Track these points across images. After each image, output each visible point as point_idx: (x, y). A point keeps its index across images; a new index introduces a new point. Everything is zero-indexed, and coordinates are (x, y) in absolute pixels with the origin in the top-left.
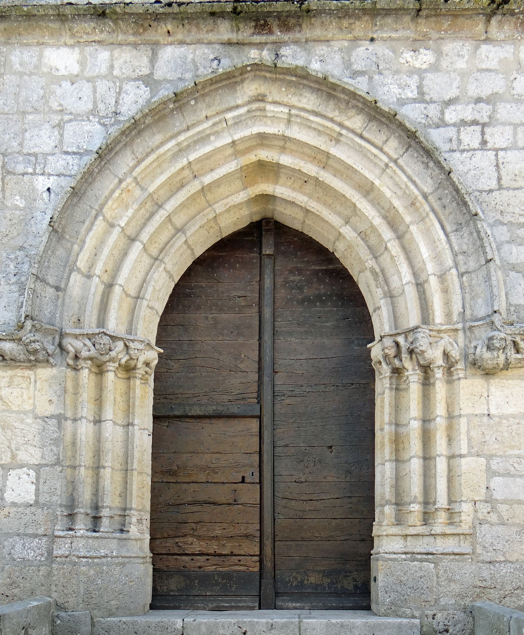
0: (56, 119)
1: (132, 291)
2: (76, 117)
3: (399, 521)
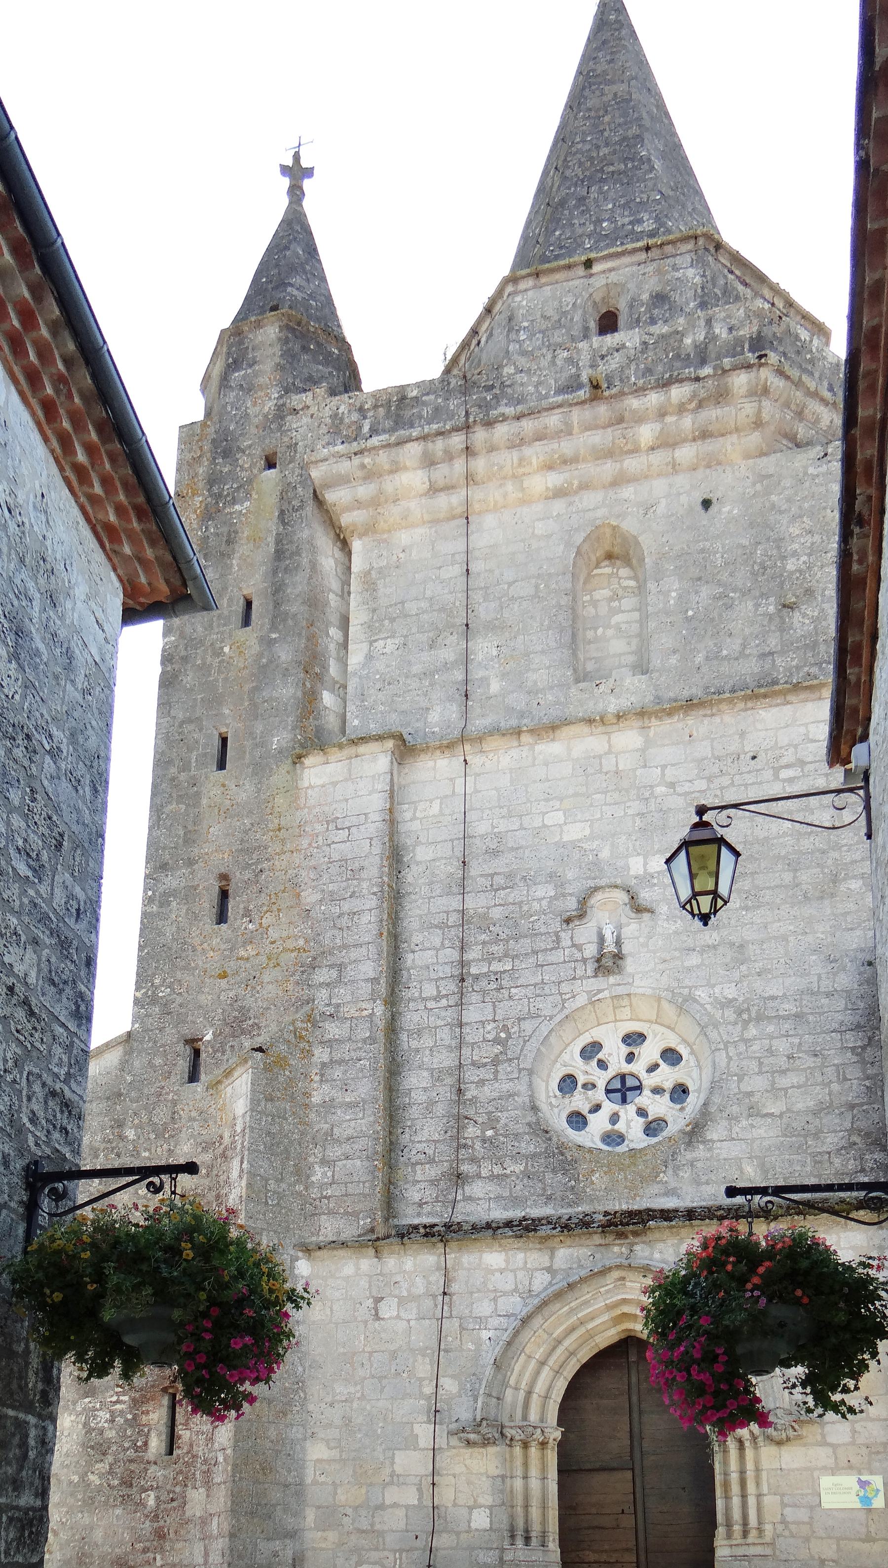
0: (492, 1295)
1: (543, 1394)
2: (505, 1294)
3: (729, 1536)
